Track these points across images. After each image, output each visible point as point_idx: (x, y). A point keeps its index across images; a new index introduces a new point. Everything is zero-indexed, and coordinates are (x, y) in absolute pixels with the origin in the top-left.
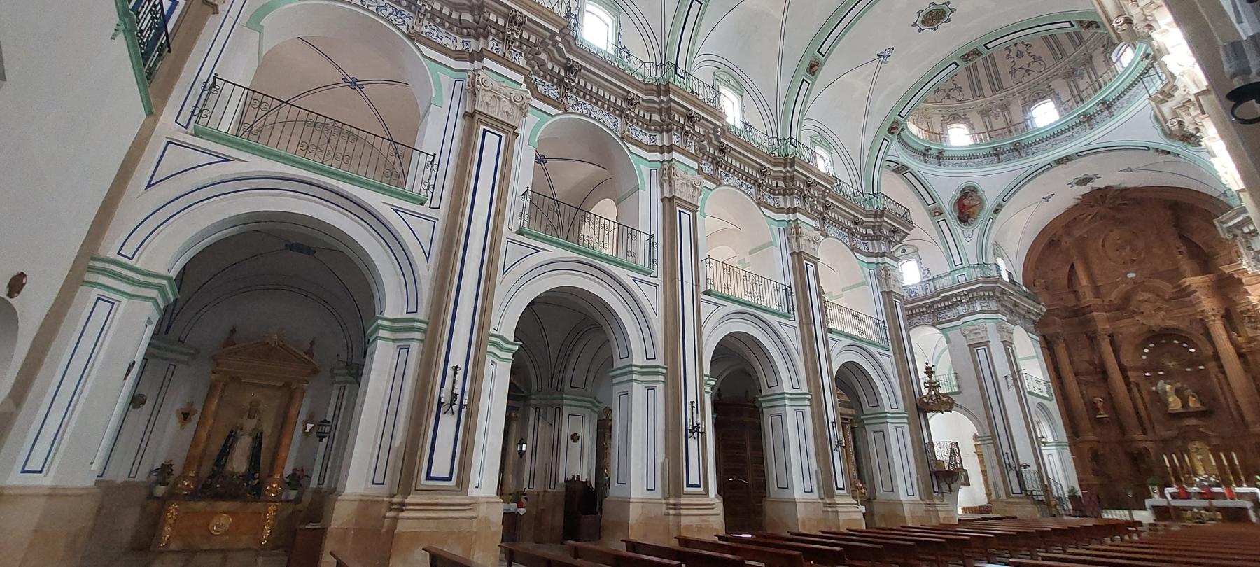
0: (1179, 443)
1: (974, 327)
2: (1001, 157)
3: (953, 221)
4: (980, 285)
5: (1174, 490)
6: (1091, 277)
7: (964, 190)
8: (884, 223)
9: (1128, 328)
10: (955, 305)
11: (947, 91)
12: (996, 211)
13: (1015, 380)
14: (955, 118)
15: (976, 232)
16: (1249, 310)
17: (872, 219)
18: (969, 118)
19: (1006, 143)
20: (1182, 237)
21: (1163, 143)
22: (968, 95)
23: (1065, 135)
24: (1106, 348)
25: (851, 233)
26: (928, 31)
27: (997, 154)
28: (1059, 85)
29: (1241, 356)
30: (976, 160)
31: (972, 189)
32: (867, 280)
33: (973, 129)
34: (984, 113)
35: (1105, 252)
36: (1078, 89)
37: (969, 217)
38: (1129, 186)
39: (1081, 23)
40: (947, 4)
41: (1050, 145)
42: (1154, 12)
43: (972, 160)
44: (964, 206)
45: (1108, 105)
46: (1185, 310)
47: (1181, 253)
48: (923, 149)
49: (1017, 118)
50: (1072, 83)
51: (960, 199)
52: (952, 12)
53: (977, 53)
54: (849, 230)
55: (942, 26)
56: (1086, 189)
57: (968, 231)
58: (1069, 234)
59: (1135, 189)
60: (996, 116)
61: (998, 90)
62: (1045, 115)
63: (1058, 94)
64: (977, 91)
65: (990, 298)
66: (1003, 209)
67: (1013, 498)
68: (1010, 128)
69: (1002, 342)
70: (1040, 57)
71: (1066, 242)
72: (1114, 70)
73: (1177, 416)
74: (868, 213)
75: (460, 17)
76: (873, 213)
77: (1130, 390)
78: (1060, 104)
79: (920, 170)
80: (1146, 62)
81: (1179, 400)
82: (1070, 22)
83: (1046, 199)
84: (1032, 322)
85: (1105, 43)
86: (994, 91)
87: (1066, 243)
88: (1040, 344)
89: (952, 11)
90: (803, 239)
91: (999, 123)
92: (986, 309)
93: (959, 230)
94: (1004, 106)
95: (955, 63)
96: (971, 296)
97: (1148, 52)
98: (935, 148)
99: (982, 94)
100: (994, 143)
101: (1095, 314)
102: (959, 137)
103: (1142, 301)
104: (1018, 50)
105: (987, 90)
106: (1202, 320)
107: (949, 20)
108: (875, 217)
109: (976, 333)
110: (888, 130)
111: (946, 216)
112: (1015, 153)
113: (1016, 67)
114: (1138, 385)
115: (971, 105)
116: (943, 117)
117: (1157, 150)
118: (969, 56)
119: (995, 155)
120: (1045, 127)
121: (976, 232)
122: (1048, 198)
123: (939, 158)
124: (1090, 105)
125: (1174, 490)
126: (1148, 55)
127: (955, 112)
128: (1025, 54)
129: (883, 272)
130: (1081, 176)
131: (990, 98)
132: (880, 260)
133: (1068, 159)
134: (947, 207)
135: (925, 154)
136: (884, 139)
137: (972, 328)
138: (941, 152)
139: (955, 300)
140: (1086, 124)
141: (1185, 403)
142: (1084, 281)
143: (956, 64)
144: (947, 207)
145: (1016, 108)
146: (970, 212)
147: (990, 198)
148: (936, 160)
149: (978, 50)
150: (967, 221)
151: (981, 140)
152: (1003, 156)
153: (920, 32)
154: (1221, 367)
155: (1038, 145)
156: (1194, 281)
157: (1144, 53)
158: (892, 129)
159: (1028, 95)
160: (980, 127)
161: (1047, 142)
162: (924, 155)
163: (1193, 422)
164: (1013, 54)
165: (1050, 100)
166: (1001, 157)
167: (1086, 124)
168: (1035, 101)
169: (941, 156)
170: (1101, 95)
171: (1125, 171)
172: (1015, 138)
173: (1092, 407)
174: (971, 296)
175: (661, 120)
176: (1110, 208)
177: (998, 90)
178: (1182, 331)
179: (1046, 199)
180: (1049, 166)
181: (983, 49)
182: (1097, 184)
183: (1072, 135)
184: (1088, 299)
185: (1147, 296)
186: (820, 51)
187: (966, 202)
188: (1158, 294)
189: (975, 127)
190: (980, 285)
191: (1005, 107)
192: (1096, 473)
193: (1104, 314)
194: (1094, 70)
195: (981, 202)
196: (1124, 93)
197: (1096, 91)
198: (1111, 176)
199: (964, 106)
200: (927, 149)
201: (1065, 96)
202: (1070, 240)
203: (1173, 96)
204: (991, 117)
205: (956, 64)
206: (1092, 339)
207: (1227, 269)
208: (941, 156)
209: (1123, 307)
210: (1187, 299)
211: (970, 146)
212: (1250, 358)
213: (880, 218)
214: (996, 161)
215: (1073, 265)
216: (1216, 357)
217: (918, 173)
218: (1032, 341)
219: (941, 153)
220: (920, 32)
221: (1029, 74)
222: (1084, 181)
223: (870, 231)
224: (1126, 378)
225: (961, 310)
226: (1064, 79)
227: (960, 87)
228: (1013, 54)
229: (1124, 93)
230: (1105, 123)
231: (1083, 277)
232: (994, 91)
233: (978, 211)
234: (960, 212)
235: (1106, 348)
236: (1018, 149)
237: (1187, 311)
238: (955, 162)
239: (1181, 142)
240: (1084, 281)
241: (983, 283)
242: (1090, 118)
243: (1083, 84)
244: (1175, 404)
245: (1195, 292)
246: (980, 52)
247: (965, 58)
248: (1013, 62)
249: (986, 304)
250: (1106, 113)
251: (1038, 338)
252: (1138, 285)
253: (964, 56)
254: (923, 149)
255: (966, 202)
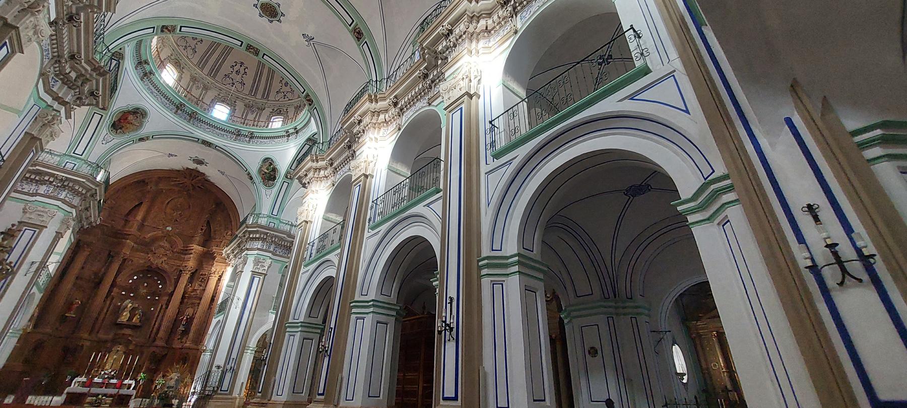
0: (104, 347)
1: (42, 209)
2: (179, 112)
3: (108, 121)
4: (84, 180)
5: (83, 379)
6: (144, 219)
7: (138, 109)
8: (94, 81)
9: (140, 259)
10: (43, 182)
11: (188, 45)
12: (141, 139)
13: (38, 269)
14: (178, 65)
15: (116, 141)
16: (205, 274)
17: (89, 68)
18: (183, 73)
19: (190, 107)
20: (208, 223)
21: (254, 171)
22: (196, 61)
23: (221, 132)
24: (115, 267)
25: (57, 59)
26: (257, 11)
27: (179, 108)
28: (240, 105)
29: (183, 297)
30: (164, 99)
31: (143, 113)
32: (23, 111)
33: (180, 81)
34: (194, 79)
35: (166, 207)
36: (259, 118)
37: (121, 128)
38: (212, 180)
39: (308, 95)
40: (283, 15)
41: (209, 130)
42: (372, 128)
43: (162, 97)
44: (126, 119)
45: (252, 136)
46: (178, 261)
47: (202, 229)
48: (144, 58)
49: (207, 100)
50: (246, 111)
51: (129, 112)
52: (278, 21)
53: (256, 52)
54: (58, 56)
55: (265, 20)
56: (193, 166)
57: (110, 137)
58: (157, 184)
59: (213, 184)
60: (198, 88)
61: (212, 76)
62: (221, 112)
63: (235, 110)
64: (202, 64)
65: (78, 193)
66: (147, 141)
67: (220, 394)
68: (198, 101)
69: (56, 232)
70: (244, 84)
71: (151, 187)
72: (644, 182)
73: (121, 326)
74: (93, 61)
75: (70, 72)
76: (97, 65)
77: (107, 297)
78: (232, 115)
79: (128, 69)
80: (284, 134)
81: (129, 315)
82: (305, 90)
83: (170, 155)
84: (80, 226)
85: (275, 109)
86: (209, 74)
87: (151, 188)
88: (71, 246)
89: (279, 21)
90: (32, 19)
91: (196, 92)
92: (68, 201)
93: (104, 131)
94: (206, 87)
95: (242, 42)
96: (64, 184)
97: (289, 131)
98: (152, 66)
99: (202, 69)
100: (184, 100)
101: (128, 241)
102: (169, 76)
103: (162, 247)
104: (239, 70)
105: (207, 69)
106: (181, 271)
107: (271, 22)
108: (94, 70)
109: (39, 215)
110: (163, 26)
111: (107, 114)
112: (188, 117)
113: (231, 76)
114: (113, 298)
115: (192, 67)
116: (172, 55)
117: (249, 174)
118: (252, 49)
119: (177, 107)
120: (215, 118)
121: (116, 141)
122: (172, 155)
123: (145, 74)
124: (245, 129)
125: (83, 379)
126: (288, 132)
127: (180, 61)
128: (240, 75)
129: (50, 118)
130: (201, 158)
131: (203, 74)
132: (56, 105)
133: (210, 145)
134: (114, 109)
135: (141, 63)
136: (154, 28)
137: (39, 208)
138: (151, 73)
139: (46, 178)
140: (235, 136)
141: (130, 319)
142: (139, 217)
143: (241, 44)
144: (114, 109)
145: (211, 94)
146: (126, 126)
147: (148, 128)
148: (142, 74)
149: (259, 52)
150: (117, 130)
151: (179, 92)
152: (181, 112)
153: (284, 15)
154: (169, 301)
155: (203, 125)
156: (196, 248)
157: (288, 130)
158: (167, 28)
159: (223, 95)
160: (184, 83)
161: (209, 127)
162: (140, 63)
163: (128, 331)
164: (236, 68)
165: (229, 108)
166: (179, 112)
167: (235, 136)
168: (223, 102)
169: (149, 74)
170: (254, 130)
171: (222, 172)
172: (196, 109)
173: (69, 305)
174: (64, 184)
175: (75, 79)
176: (192, 184)
177: (212, 76)
178: (165, 272)
179: (170, 155)
180: (197, 140)
181: (261, 55)
182: (201, 168)
183: (224, 135)
184: (132, 230)
185: (167, 245)
186: (182, 28)
187: (131, 117)
188: (172, 244)
189: (182, 81)
190: (84, 180)
191: (206, 88)
192: (26, 361)
193: (133, 244)
194: (260, 115)
195: (141, 125)
196: (262, 138)
197: (253, 125)
198: (211, 172)
199: (188, 63)
200: (146, 62)
201: (238, 113)
202: (154, 188)
203: (318, 162)
204: (195, 85)
205: (241, 44)
206: (110, 257)
207: (214, 249)
208: (149, 74)
209: (146, 246)
210: (183, 256)
211: (170, 88)
212: (186, 300)
213: (97, 74)
214: (174, 111)
215: (142, 203)
216: (171, 294)
217: (124, 69)
218: (68, 241)
219: (151, 73)
220: (254, 6)
221: (232, 86)
222: (200, 162)
223: (73, 75)
224: (110, 291)
225: (43, 189)
226: (245, 105)
227: (196, 52)
228: (236, 68)
229: (262, 138)
230: (243, 143)
231: (141, 215)
232: (209, 74)
233: (131, 130)
234: (119, 120)
235: (115, 267)
236: (192, 117)
237: (178, 263)
238: (151, 87)
239: (261, 179)
240: (139, 217)
241: (88, 180)
242: (239, 135)
243: (251, 117)
244: (124, 317)
245: (191, 254)
246: (258, 54)
247: (249, 47)
248: (232, 72)
249: (71, 196)
250: (247, 139)
251: (73, 240)
252: (167, 236)
253: (251, 46)
254: (144, 58)
255: (131, 117)
